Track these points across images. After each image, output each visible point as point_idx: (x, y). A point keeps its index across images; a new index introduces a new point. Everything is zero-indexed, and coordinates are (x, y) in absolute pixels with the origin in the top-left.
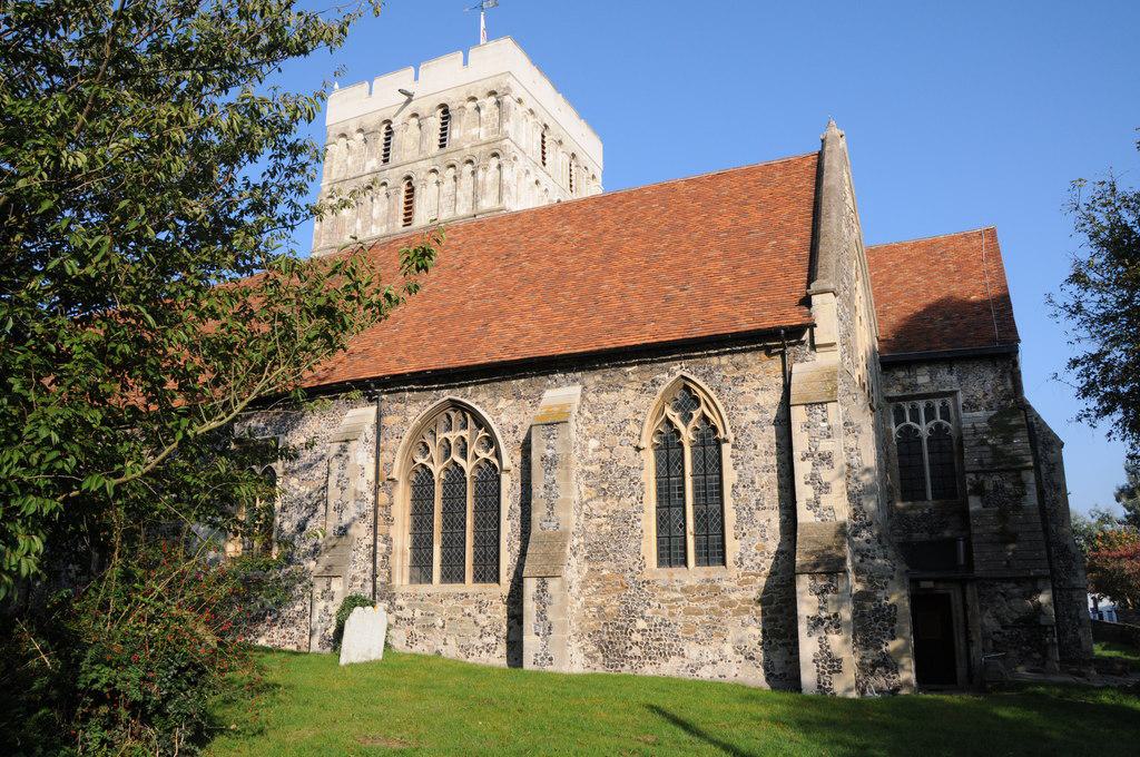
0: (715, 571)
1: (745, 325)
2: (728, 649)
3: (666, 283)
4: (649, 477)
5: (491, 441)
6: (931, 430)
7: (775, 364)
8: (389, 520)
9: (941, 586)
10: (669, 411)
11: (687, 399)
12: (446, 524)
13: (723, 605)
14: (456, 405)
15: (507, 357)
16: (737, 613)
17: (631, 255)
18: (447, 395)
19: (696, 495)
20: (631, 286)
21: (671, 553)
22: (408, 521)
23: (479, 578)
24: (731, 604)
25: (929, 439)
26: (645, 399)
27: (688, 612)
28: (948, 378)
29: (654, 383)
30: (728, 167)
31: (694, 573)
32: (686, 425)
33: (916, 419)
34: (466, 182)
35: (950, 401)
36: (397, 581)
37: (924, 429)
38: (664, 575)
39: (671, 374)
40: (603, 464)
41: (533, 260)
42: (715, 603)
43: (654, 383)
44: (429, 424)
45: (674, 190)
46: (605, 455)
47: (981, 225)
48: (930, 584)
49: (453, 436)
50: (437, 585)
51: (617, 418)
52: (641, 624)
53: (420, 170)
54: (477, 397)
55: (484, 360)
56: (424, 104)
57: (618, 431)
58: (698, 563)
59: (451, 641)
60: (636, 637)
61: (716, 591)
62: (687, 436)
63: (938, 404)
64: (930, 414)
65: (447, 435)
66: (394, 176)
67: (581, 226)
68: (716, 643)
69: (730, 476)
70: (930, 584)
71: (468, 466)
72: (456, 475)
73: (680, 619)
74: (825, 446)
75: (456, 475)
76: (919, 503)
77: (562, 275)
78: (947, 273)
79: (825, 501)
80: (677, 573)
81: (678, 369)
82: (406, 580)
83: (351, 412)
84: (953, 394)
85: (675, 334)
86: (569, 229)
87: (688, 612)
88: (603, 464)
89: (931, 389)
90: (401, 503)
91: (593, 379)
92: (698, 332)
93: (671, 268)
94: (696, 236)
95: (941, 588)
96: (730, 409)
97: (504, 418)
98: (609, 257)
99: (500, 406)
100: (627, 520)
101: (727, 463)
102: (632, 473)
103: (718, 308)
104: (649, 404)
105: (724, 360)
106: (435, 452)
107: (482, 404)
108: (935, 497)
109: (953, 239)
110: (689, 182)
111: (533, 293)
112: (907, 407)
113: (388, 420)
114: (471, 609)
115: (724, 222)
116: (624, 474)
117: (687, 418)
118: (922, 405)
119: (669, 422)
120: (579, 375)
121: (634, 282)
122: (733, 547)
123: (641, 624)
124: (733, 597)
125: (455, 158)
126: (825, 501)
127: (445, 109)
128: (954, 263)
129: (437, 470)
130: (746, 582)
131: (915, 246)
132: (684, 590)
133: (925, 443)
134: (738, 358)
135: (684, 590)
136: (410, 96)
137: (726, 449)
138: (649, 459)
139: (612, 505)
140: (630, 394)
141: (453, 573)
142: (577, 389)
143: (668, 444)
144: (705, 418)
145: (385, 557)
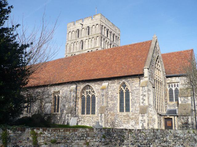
0: (128, 113)
1: (133, 74)
2: (130, 125)
3: (123, 65)
4: (118, 98)
5: (93, 92)
6: (175, 89)
7: (138, 80)
8: (78, 104)
9: (171, 117)
10: (122, 87)
11: (124, 85)
12: (87, 103)
13: (129, 118)
14: (88, 85)
15: (97, 78)
16: (131, 120)
17: (118, 60)
18: (87, 84)
19: (126, 101)
20: (117, 66)
21: (121, 110)
22: (81, 104)
23: (92, 114)
24: (131, 118)
25: (175, 91)
26: (118, 85)
27: (124, 119)
28: (178, 79)
29: (120, 83)
30: (136, 42)
31: (125, 113)
32: (124, 89)
33: (172, 87)
34: (93, 41)
35: (178, 83)
36: (79, 114)
37: (174, 89)
38: (120, 113)
39: (122, 81)
40: (112, 95)
41: (102, 60)
42: (128, 118)
43: (120, 83)
44: (84, 88)
45: (127, 47)
46: (112, 94)
47: (190, 48)
48: (169, 116)
49: (88, 91)
50: (85, 115)
51: (114, 88)
52: (117, 121)
53: (84, 39)
54: (92, 85)
55: (93, 78)
56: (85, 26)
57: (114, 90)
58: (126, 112)
59: (88, 124)
60: (116, 123)
61: (128, 116)
62: (124, 91)
63: (176, 84)
64: (175, 86)
65: (87, 90)
66: (79, 40)
67: (111, 54)
68: (128, 124)
69: (131, 98)
70: (169, 116)
71: (91, 95)
72: (88, 96)
73: (123, 120)
74: (145, 93)
75: (88, 96)
76: (172, 102)
77: (106, 63)
78: (182, 59)
79: (144, 102)
80: (123, 113)
81: (124, 80)
82: (81, 114)
83: (72, 86)
84: (179, 82)
85: (123, 75)
86: (109, 54)
87: (124, 119)
88: (112, 95)
89: (175, 82)
90: (80, 102)
91: (110, 82)
92: (126, 75)
93: (124, 63)
94: (129, 56)
95: (171, 117)
96: (131, 87)
97: (96, 88)
98: (115, 60)
99: (96, 86)
100: (115, 104)
101: (130, 96)
102: (116, 97)
103: (130, 70)
104: (118, 86)
105: (130, 79)
106: (85, 93)
107: (93, 85)
108: (175, 101)
109: (185, 51)
110: (130, 45)
111: (102, 66)
112: (171, 84)
113: (78, 88)
114: (91, 119)
115: (134, 54)
116: (115, 97)
117: (124, 88)
118: (173, 84)
119: (121, 89)
120: (108, 81)
121: (118, 65)
122: (131, 109)
123: (117, 121)
124: (131, 117)
125: (91, 37)
126: (144, 102)
127: (88, 27)
128: (184, 56)
129: (86, 96)
130: (133, 115)
131: (177, 53)
132: (123, 116)
133: (86, 99)
134: (132, 79)
135: (123, 116)
136: (82, 25)
137: (130, 94)
138: (118, 95)
139: (113, 102)
140: (116, 84)
141: (88, 113)
142: (108, 83)
143: (121, 93)
144: (127, 88)
145: (77, 110)
